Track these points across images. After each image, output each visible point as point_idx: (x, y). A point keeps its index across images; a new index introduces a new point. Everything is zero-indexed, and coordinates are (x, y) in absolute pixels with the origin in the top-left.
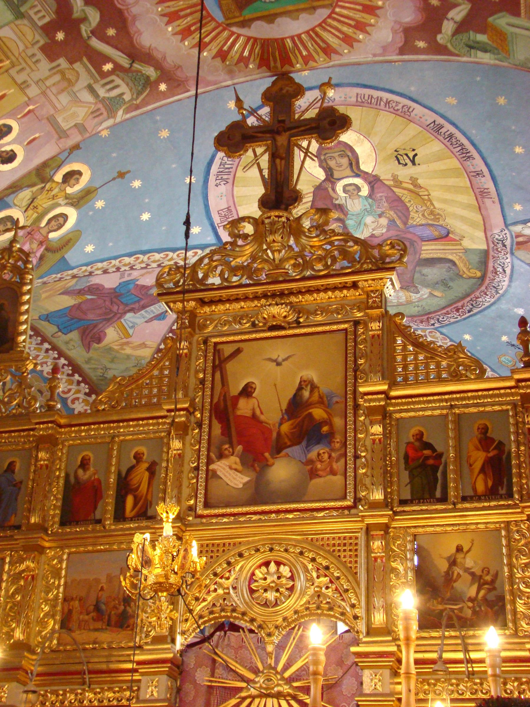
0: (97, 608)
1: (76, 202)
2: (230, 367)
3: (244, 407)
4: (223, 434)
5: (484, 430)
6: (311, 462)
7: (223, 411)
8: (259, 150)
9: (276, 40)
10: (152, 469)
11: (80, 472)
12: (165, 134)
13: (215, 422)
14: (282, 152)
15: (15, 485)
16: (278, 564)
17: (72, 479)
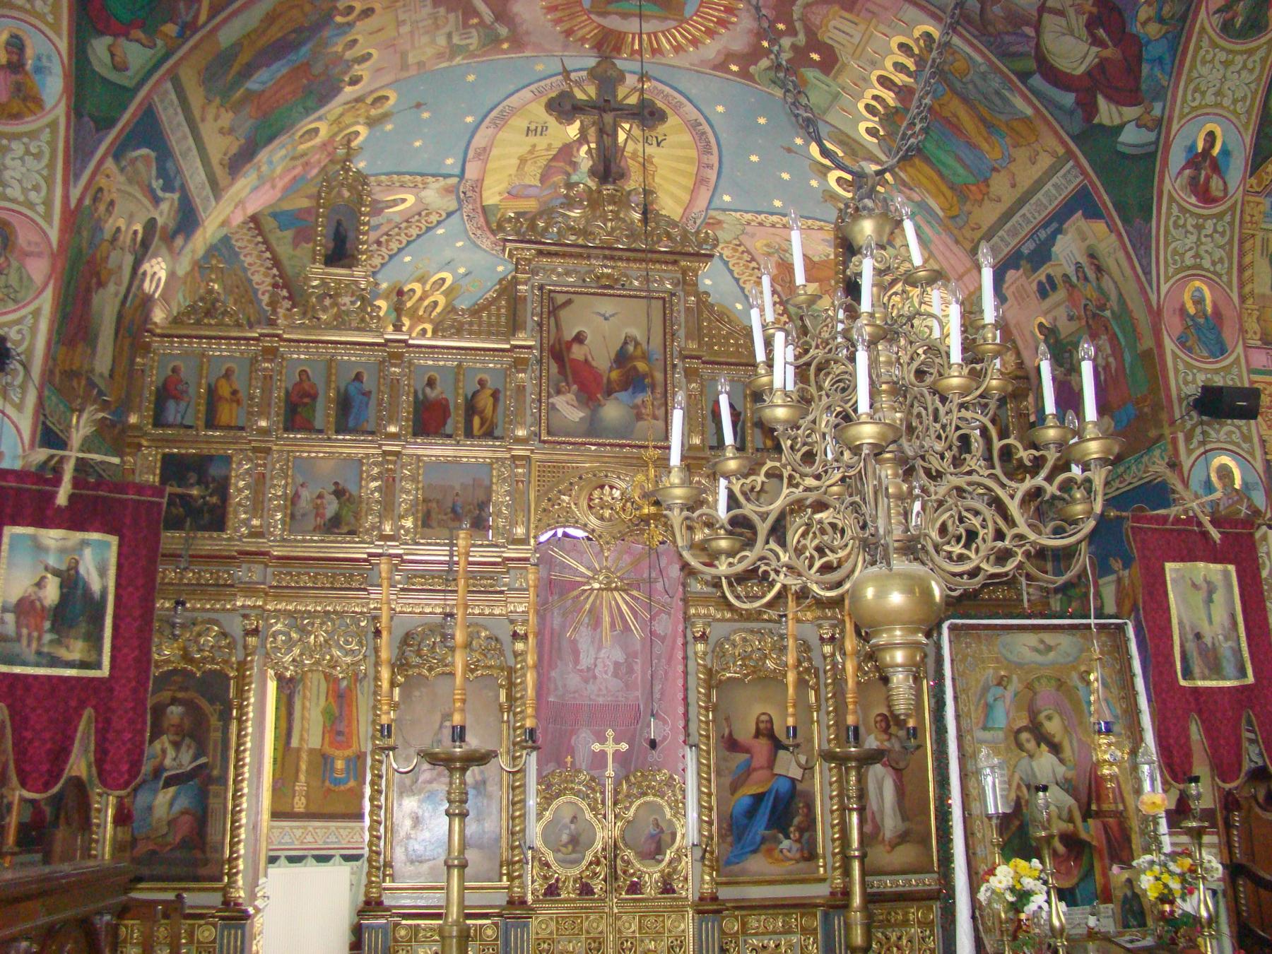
0: (454, 511)
1: (372, 123)
2: (563, 314)
3: (577, 352)
4: (559, 372)
6: (636, 407)
7: (558, 352)
9: (620, 33)
10: (495, 395)
11: (428, 390)
12: (471, 78)
13: (552, 363)
14: (609, 129)
15: (364, 394)
16: (612, 487)
17: (421, 397)
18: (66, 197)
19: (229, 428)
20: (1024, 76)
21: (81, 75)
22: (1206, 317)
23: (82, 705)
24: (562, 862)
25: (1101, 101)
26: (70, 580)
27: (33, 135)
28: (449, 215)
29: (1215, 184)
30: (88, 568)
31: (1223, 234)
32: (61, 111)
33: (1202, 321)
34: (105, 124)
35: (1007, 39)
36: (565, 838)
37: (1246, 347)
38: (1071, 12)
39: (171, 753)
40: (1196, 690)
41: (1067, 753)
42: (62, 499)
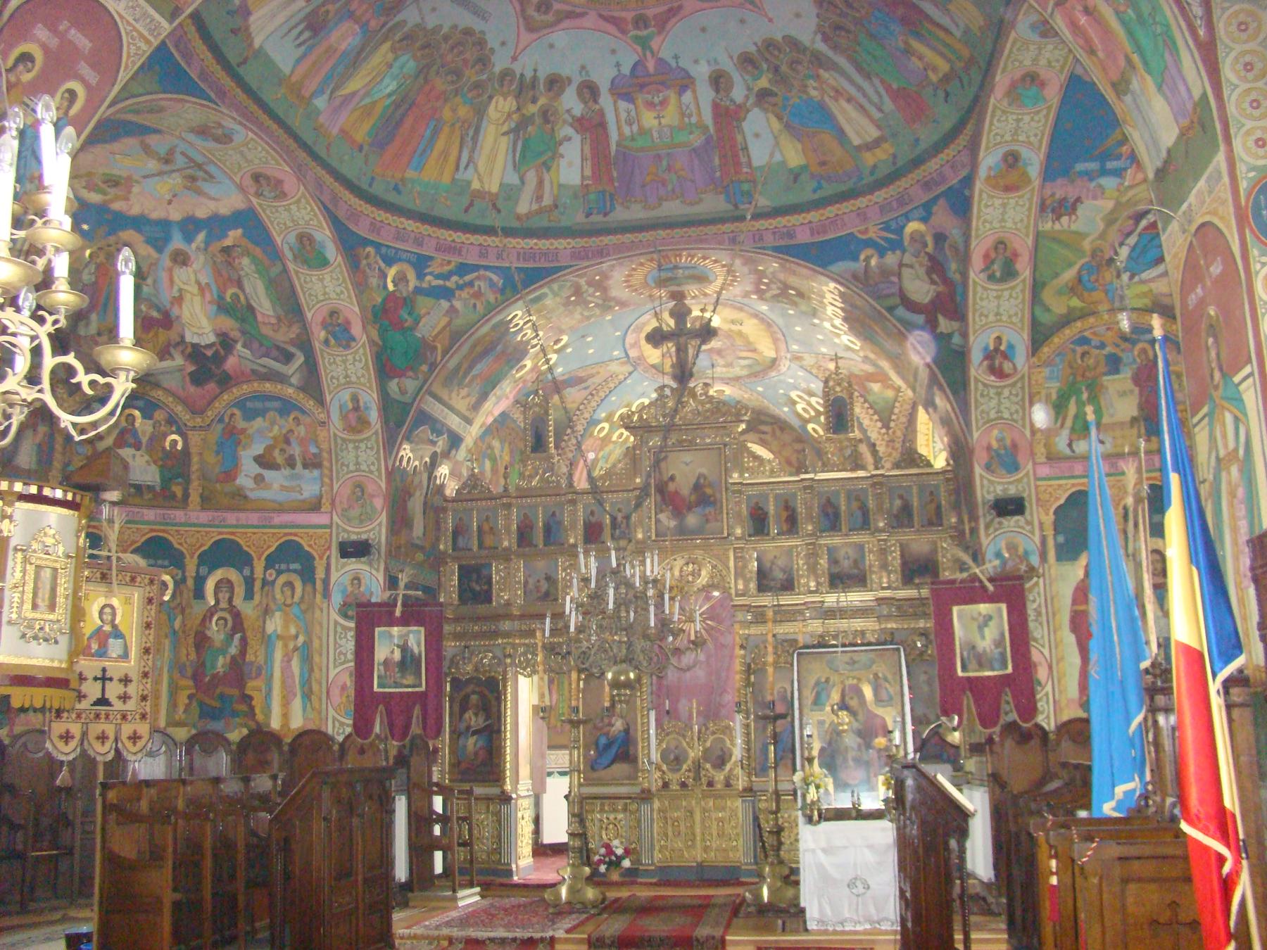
2: (663, 465)
3: (672, 487)
5: (786, 501)
6: (705, 515)
8: (670, 345)
18: (387, 468)
19: (490, 548)
20: (891, 309)
21: (386, 403)
22: (1005, 448)
23: (414, 704)
24: (671, 770)
25: (941, 319)
26: (404, 648)
27: (368, 439)
28: (630, 374)
29: (1007, 367)
30: (412, 642)
31: (1017, 395)
32: (379, 426)
33: (1002, 452)
34: (399, 425)
35: (882, 286)
36: (672, 757)
37: (1035, 464)
38: (917, 266)
39: (473, 719)
40: (968, 679)
41: (860, 717)
42: (398, 613)
